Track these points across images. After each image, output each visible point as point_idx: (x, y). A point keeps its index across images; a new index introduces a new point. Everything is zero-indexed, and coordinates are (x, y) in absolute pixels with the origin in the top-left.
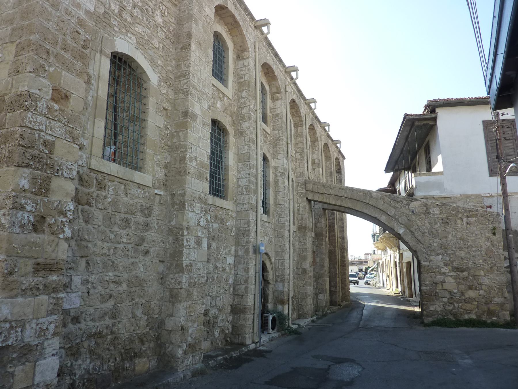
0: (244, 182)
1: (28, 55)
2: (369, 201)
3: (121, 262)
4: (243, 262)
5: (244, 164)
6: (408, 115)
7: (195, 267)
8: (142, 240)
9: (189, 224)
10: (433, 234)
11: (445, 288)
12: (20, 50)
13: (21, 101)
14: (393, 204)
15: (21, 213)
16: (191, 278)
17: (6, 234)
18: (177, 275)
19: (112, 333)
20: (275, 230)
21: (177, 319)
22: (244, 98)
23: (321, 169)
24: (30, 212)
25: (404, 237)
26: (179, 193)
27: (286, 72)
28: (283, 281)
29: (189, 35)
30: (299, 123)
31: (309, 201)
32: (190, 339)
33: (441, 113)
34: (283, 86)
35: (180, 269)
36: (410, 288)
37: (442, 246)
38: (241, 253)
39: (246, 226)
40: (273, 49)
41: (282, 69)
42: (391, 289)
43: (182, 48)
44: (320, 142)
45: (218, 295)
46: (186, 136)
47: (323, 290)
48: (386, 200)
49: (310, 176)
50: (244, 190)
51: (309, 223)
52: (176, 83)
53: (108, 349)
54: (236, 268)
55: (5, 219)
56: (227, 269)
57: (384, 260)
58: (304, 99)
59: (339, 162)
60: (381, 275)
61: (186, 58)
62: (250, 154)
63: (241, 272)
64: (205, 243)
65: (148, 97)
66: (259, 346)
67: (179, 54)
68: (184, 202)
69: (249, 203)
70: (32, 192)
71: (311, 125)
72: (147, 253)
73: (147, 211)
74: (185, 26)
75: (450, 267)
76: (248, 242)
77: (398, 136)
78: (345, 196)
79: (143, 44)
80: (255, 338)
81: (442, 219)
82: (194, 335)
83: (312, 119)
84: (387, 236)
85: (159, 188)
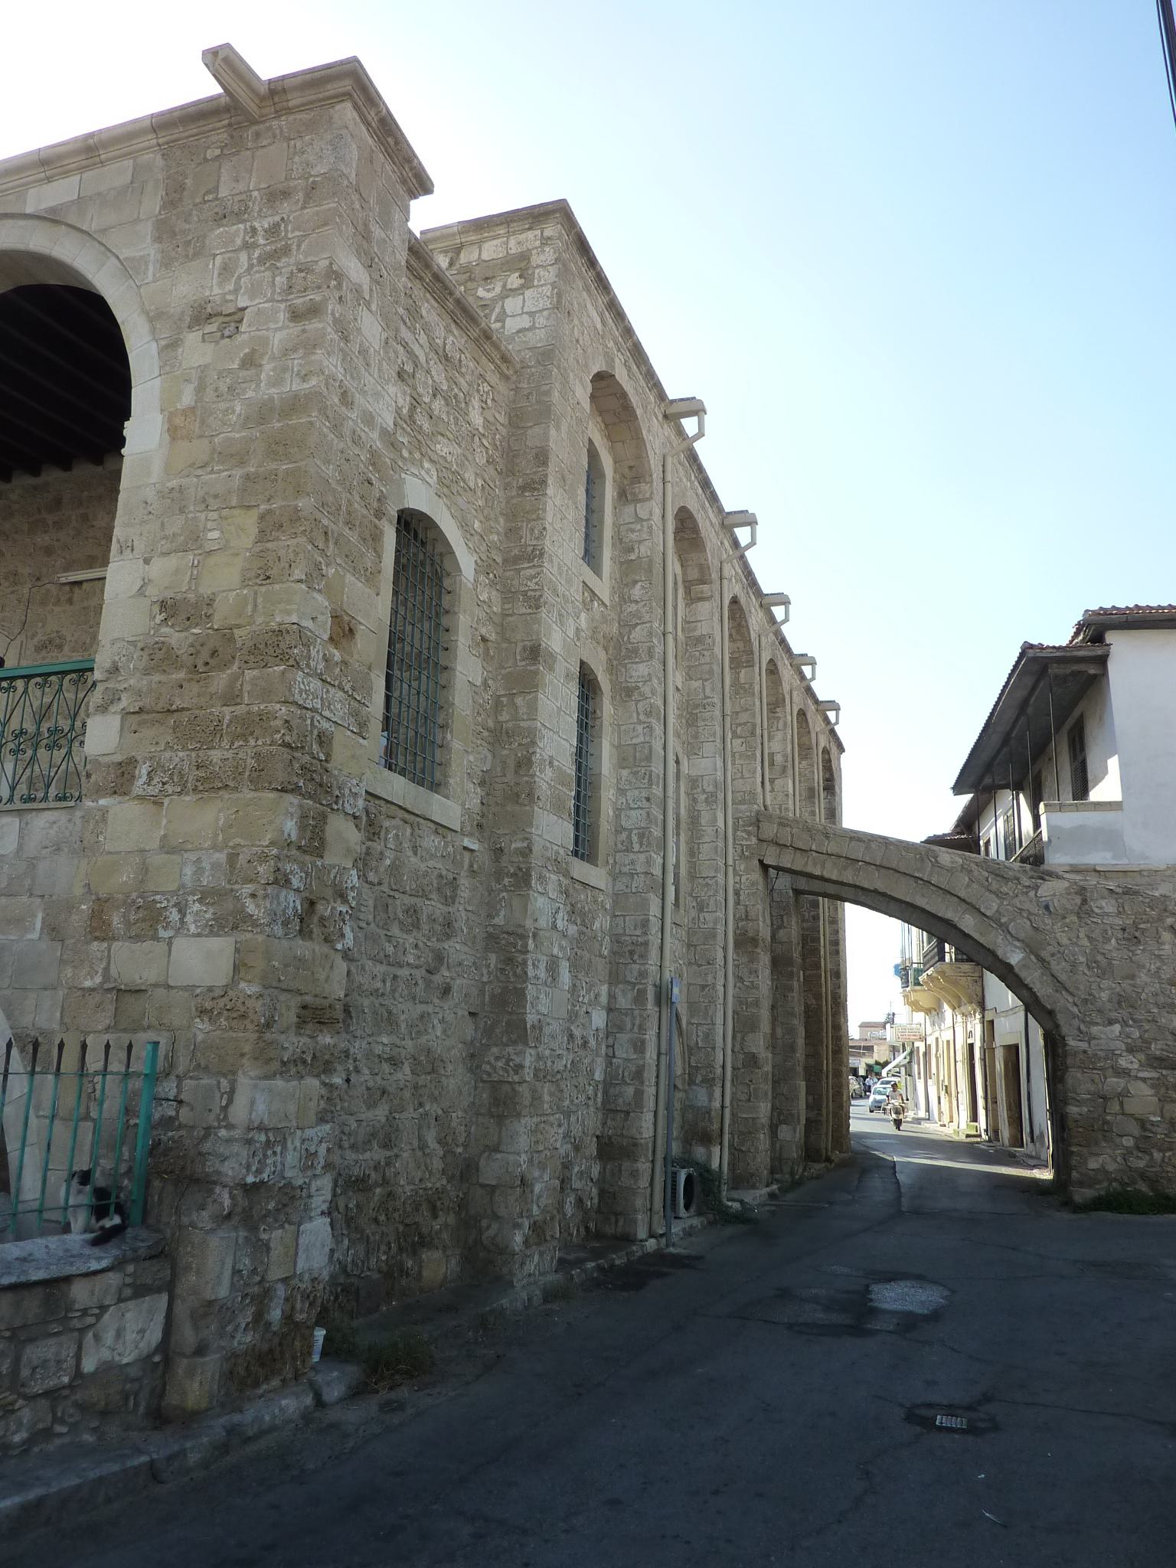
0: (634, 819)
1: (295, 541)
2: (931, 874)
3: (406, 1011)
4: (629, 1026)
5: (636, 773)
6: (1032, 646)
7: (547, 1030)
8: (439, 958)
9: (537, 925)
10: (1098, 967)
11: (1129, 1109)
12: (270, 527)
13: (282, 645)
14: (995, 886)
15: (284, 892)
16: (539, 1057)
17: (261, 938)
18: (510, 1049)
19: (385, 1182)
20: (689, 946)
21: (512, 1158)
22: (637, 602)
23: (790, 782)
24: (297, 890)
25: (1023, 974)
26: (513, 846)
27: (723, 525)
28: (709, 1082)
29: (542, 457)
30: (743, 657)
31: (765, 867)
32: (535, 1210)
33: (1122, 648)
34: (717, 563)
35: (519, 1032)
36: (1016, 1120)
37: (1120, 1000)
38: (624, 1002)
39: (638, 932)
40: (700, 469)
41: (714, 520)
42: (954, 1126)
43: (523, 488)
44: (788, 708)
45: (573, 1108)
46: (533, 707)
47: (792, 1115)
48: (976, 873)
49: (768, 802)
50: (635, 839)
51: (763, 929)
52: (508, 574)
53: (376, 1221)
54: (611, 1041)
55: (258, 906)
56: (592, 1043)
57: (931, 1040)
58: (758, 593)
59: (830, 761)
60: (920, 1084)
61: (535, 515)
62: (650, 748)
63: (623, 1052)
64: (565, 977)
65: (455, 613)
66: (667, 1246)
67: (514, 501)
68: (528, 869)
69: (646, 873)
70: (300, 847)
71: (771, 661)
72: (446, 991)
73: (448, 890)
74: (529, 432)
75: (1142, 1057)
76: (643, 974)
77: (999, 699)
78: (867, 859)
79: (449, 484)
80: (655, 1225)
81: (1124, 930)
82: (543, 1202)
83: (773, 644)
84: (949, 972)
85: (471, 835)
